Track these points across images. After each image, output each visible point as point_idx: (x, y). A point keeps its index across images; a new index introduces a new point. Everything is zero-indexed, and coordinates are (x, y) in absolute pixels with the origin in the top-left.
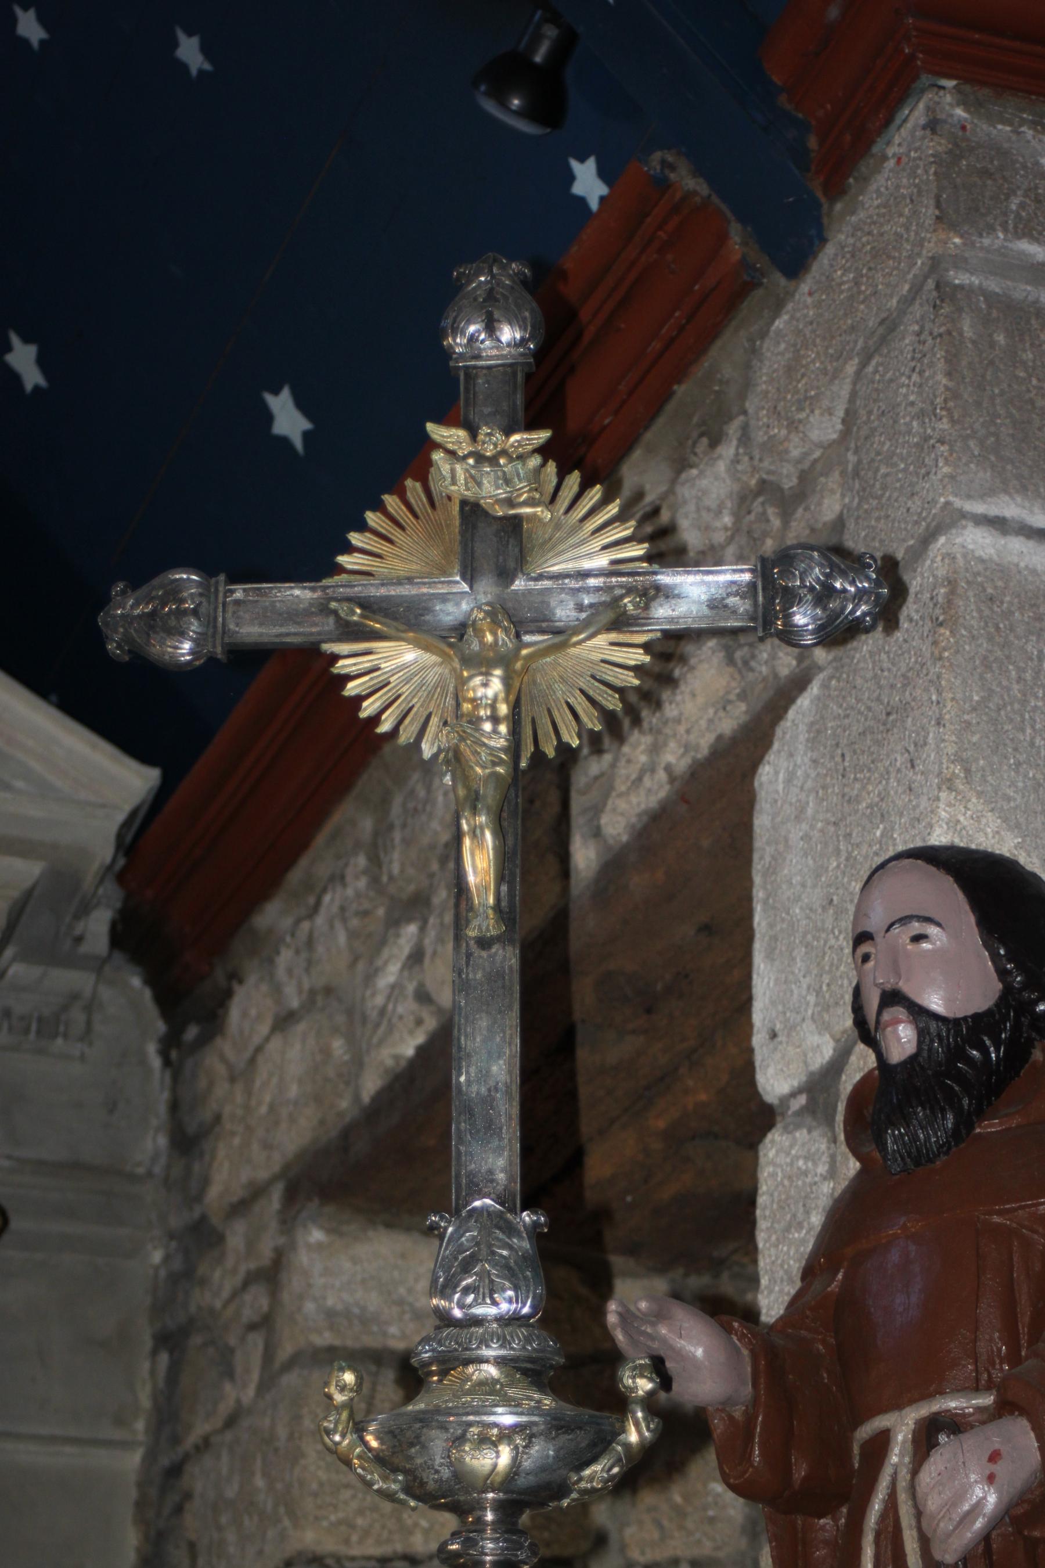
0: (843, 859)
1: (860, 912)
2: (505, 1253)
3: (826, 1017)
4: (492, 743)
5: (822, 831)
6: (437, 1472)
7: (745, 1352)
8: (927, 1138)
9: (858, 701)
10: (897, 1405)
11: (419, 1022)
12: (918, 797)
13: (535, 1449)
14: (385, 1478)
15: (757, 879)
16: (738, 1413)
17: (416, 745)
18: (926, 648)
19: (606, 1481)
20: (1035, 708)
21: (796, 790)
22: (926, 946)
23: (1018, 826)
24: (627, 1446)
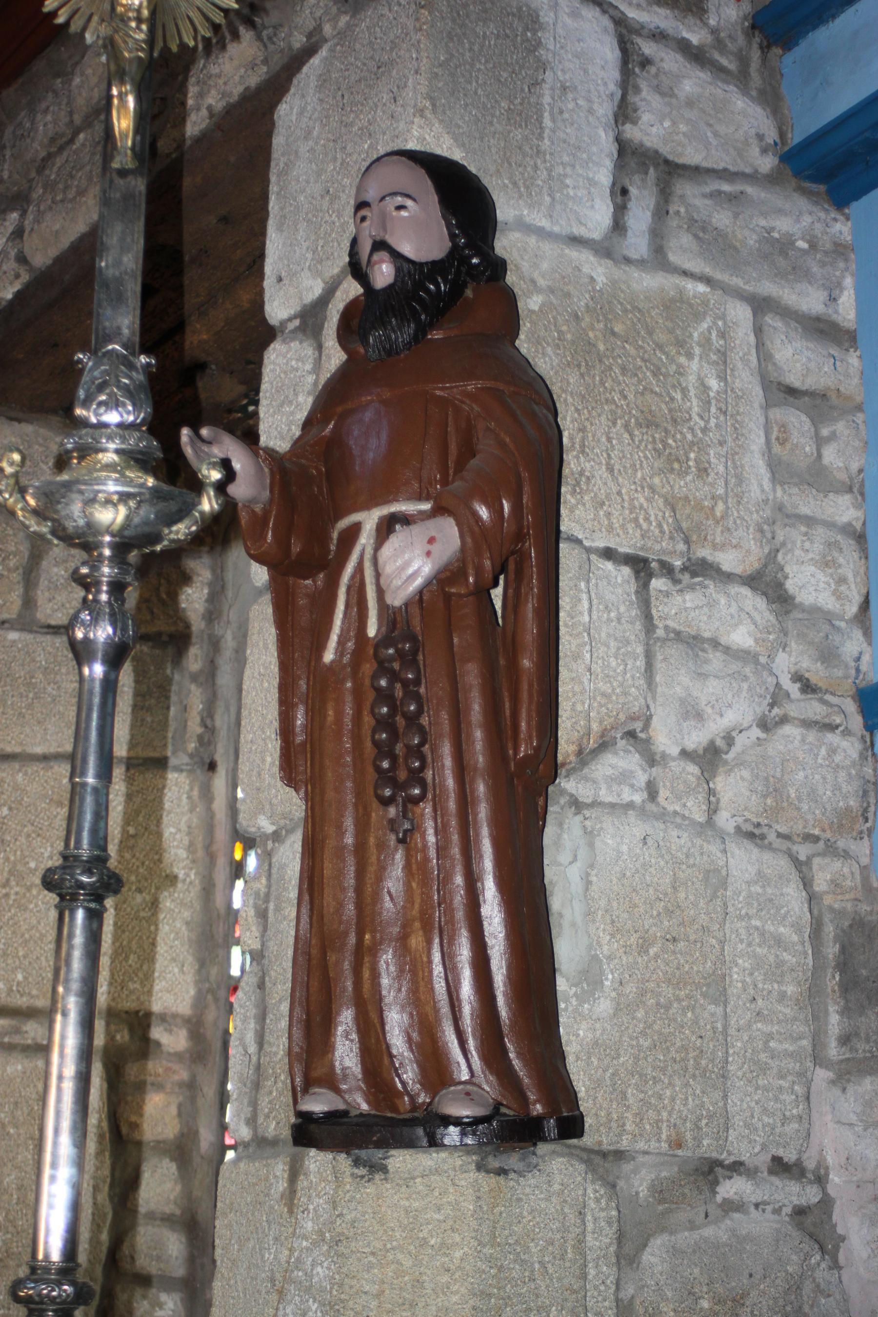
0: (338, 164)
1: (360, 189)
2: (126, 381)
3: (319, 267)
4: (137, 37)
5: (324, 146)
6: (75, 521)
7: (266, 470)
8: (397, 338)
9: (356, 59)
10: (368, 506)
11: (17, 276)
12: (397, 121)
13: (142, 512)
14: (38, 524)
15: (273, 178)
16: (258, 508)
17: (81, 35)
18: (410, 24)
19: (187, 535)
20: (479, 70)
21: (306, 120)
22: (404, 213)
23: (463, 145)
24: (202, 513)
